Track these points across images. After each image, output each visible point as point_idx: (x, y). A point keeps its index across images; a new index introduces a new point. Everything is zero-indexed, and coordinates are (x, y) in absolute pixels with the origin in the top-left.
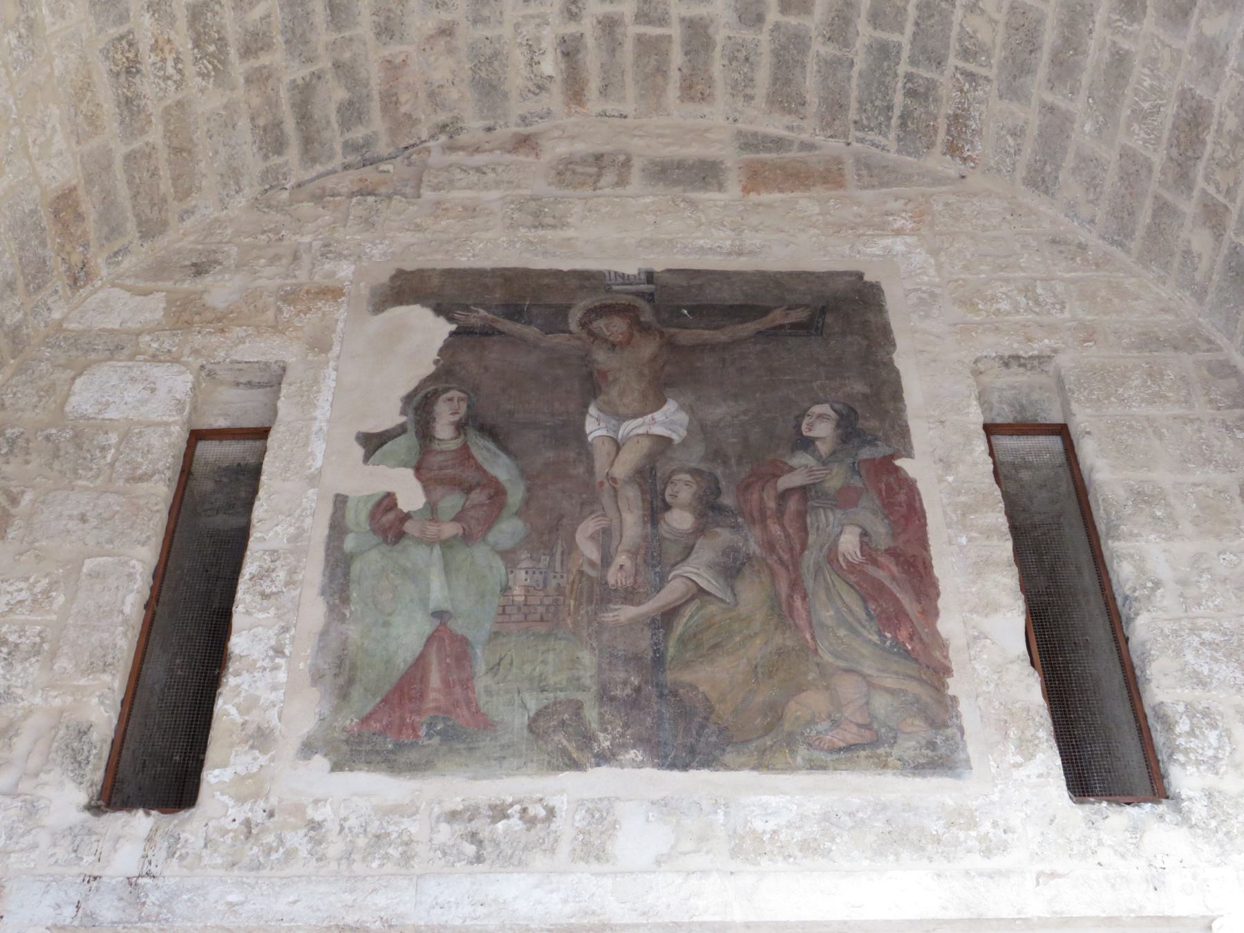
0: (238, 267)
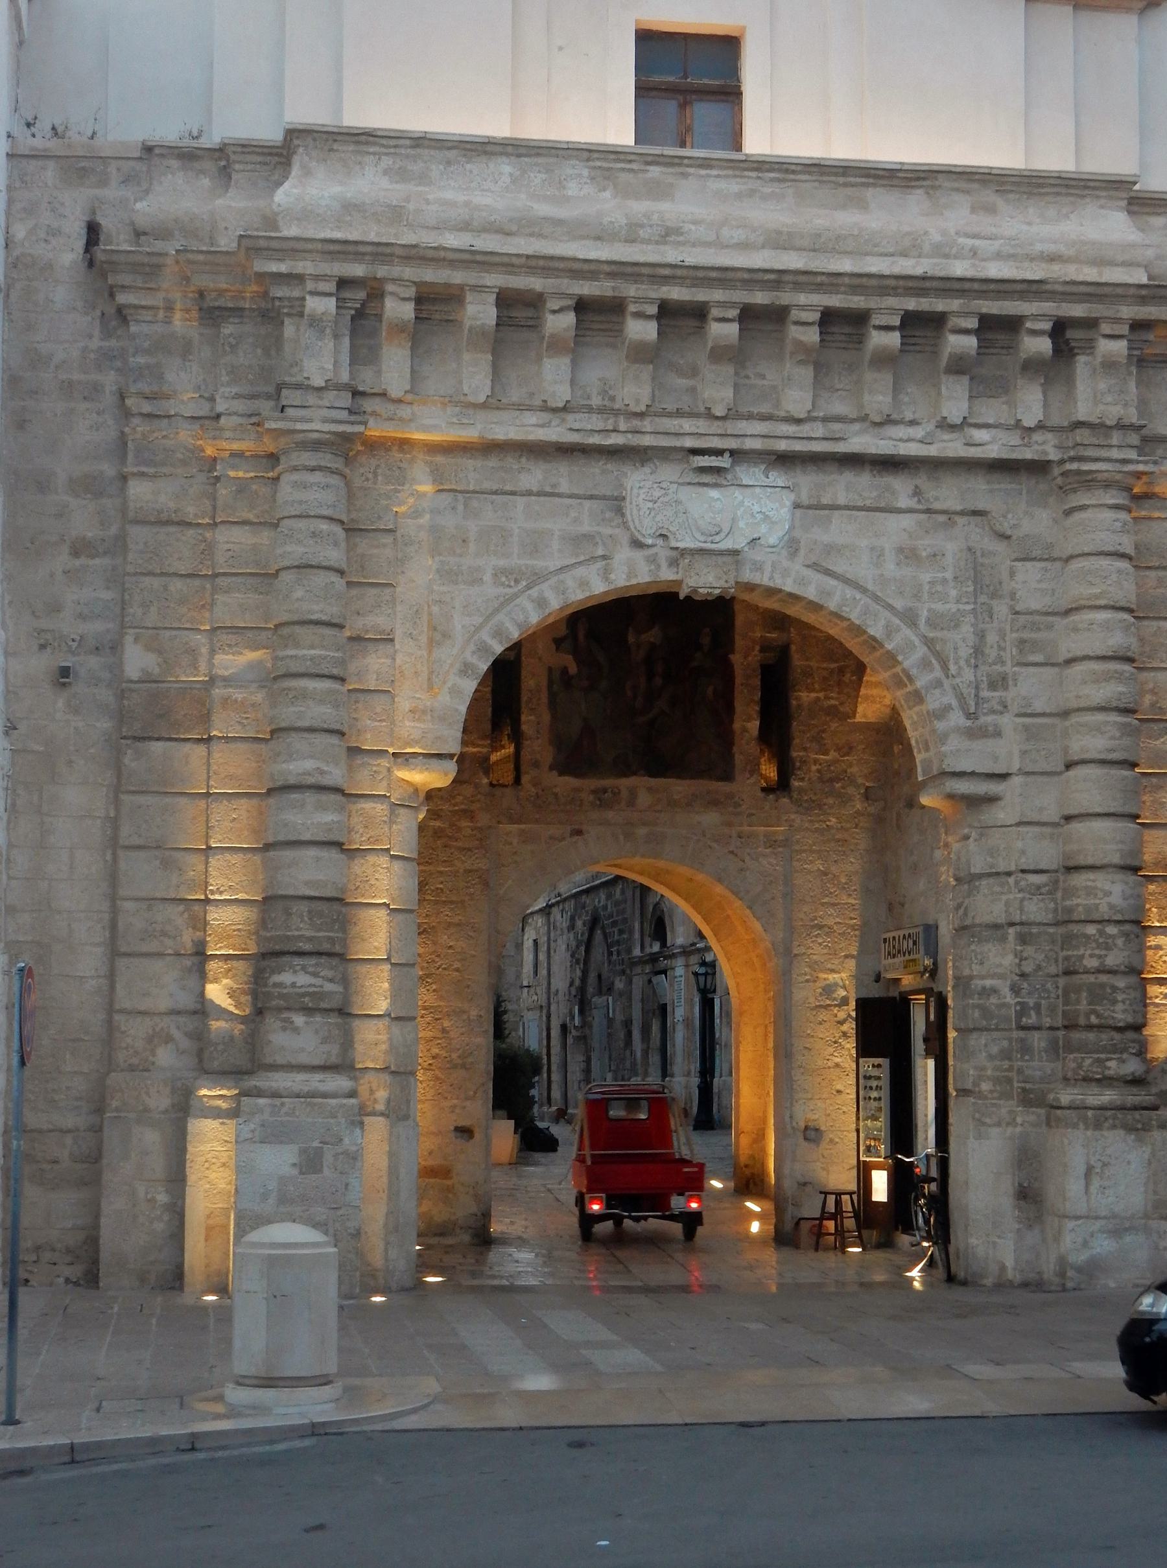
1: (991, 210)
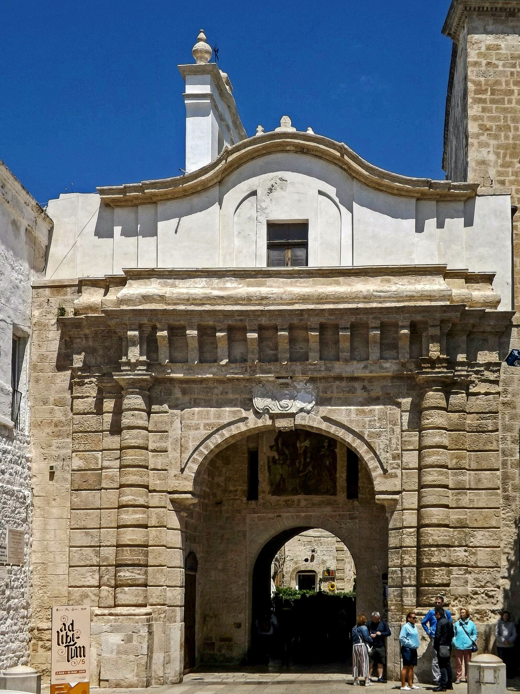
0: (198, 543)
1: (389, 281)
